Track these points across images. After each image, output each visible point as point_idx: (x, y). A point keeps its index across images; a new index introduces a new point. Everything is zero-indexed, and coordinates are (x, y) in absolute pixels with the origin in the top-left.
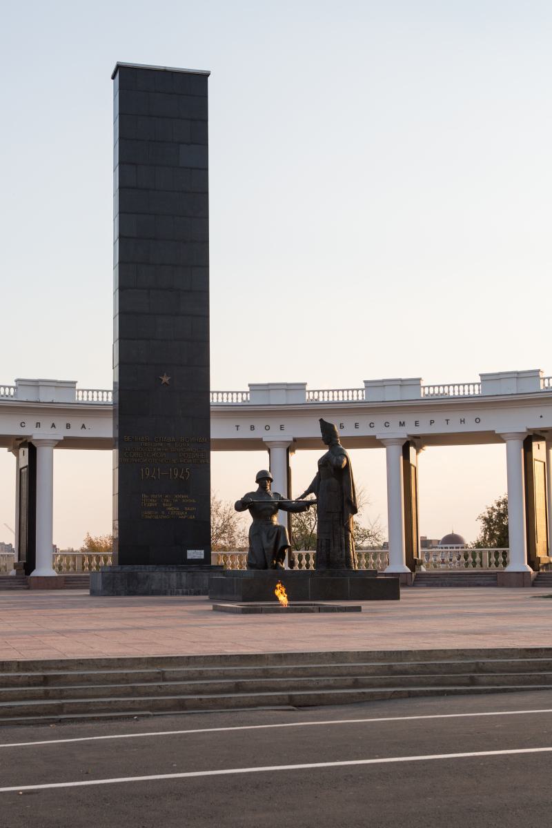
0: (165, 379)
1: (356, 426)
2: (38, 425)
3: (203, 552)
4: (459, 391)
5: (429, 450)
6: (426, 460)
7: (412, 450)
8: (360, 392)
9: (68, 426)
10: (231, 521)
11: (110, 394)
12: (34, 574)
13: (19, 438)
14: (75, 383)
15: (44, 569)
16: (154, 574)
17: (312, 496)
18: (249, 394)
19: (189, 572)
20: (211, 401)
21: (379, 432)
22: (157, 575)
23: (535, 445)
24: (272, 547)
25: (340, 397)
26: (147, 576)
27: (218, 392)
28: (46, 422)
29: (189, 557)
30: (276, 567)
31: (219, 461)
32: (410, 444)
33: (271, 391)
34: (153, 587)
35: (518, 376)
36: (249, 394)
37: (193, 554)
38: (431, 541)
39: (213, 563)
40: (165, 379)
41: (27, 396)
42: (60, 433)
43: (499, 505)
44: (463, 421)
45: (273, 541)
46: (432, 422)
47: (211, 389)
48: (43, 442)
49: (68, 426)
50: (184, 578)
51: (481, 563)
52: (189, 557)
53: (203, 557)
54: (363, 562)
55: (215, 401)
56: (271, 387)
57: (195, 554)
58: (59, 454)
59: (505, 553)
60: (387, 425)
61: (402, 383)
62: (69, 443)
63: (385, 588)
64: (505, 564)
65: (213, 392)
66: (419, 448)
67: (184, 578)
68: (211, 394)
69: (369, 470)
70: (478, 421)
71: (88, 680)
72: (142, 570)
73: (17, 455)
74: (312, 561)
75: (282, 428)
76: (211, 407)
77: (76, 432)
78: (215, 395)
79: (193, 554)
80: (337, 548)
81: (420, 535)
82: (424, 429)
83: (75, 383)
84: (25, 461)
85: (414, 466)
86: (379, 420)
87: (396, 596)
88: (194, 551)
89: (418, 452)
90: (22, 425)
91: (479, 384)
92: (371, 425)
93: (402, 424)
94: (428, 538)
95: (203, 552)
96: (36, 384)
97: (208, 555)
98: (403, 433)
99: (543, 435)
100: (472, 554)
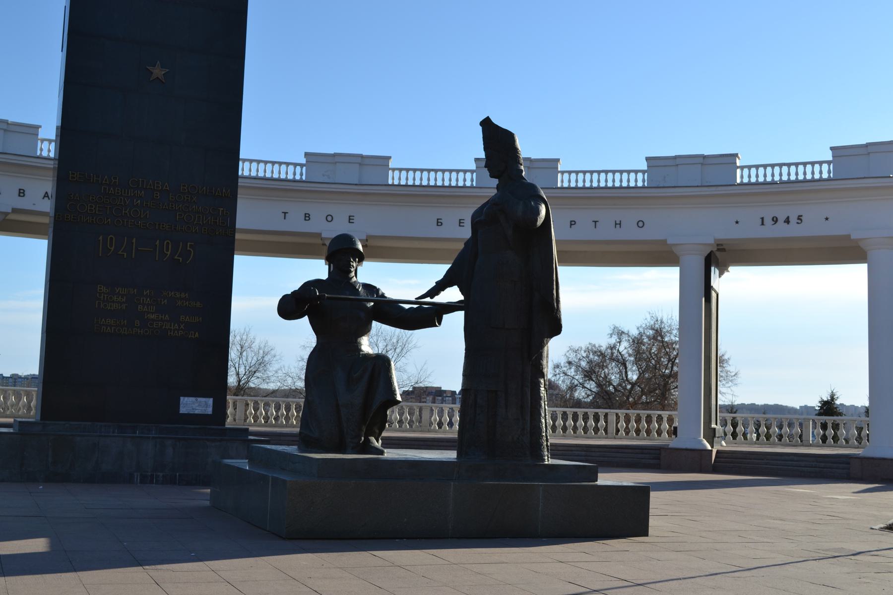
0: (158, 72)
3: (210, 401)
4: (457, 180)
5: (735, 272)
6: (735, 285)
7: (714, 272)
8: (468, 175)
10: (266, 359)
14: (38, 127)
17: (453, 294)
18: (304, 168)
20: (240, 173)
25: (610, 181)
27: (251, 161)
29: (183, 410)
30: (367, 448)
31: (244, 267)
32: (718, 257)
36: (304, 168)
37: (191, 405)
38: (445, 391)
39: (229, 423)
40: (158, 72)
46: (572, 223)
47: (242, 156)
51: (606, 430)
52: (183, 410)
53: (209, 411)
54: (435, 420)
55: (246, 173)
56: (678, 161)
57: (194, 405)
65: (244, 160)
68: (241, 163)
76: (240, 180)
78: (247, 164)
79: (191, 405)
81: (719, 403)
83: (38, 127)
85: (715, 291)
88: (193, 399)
89: (721, 274)
91: (643, 172)
94: (443, 389)
95: (210, 401)
100: (647, 417)
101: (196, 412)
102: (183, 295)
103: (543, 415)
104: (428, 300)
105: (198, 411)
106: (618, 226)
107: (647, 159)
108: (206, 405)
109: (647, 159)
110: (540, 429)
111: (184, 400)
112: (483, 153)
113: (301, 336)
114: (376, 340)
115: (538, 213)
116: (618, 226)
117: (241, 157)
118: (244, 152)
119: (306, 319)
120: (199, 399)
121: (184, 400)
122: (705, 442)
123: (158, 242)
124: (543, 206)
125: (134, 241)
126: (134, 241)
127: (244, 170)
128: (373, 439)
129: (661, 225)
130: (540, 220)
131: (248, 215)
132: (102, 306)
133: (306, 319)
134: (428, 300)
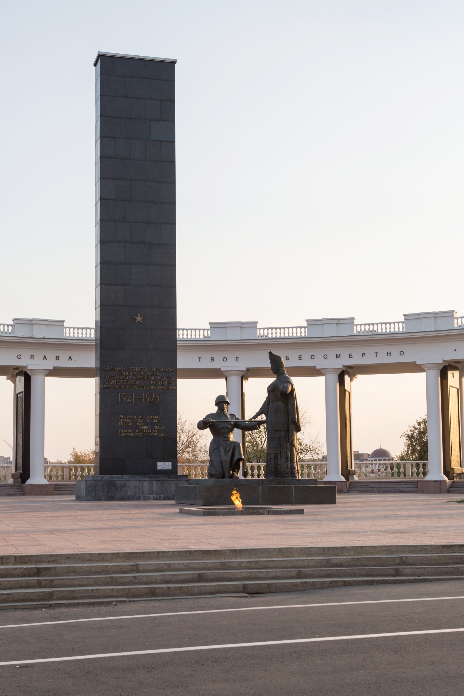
0: (139, 318)
1: (300, 358)
2: (32, 357)
3: (170, 464)
7: (347, 378)
9: (57, 358)
11: (93, 331)
12: (29, 482)
13: (16, 368)
15: (37, 478)
16: (129, 482)
17: (263, 417)
19: (159, 481)
20: (177, 337)
21: (319, 363)
22: (132, 483)
23: (450, 373)
24: (229, 459)
26: (124, 484)
28: (39, 355)
29: (159, 468)
32: (343, 374)
33: (228, 328)
34: (129, 493)
35: (436, 315)
40: (139, 318)
41: (23, 332)
42: (51, 364)
43: (419, 424)
44: (389, 354)
45: (230, 454)
46: (363, 355)
48: (36, 371)
49: (57, 358)
50: (155, 486)
52: (159, 468)
53: (170, 468)
58: (49, 381)
59: (424, 465)
60: (325, 357)
61: (338, 322)
62: (58, 372)
63: (324, 494)
64: (425, 474)
65: (179, 330)
66: (352, 377)
67: (155, 486)
68: (177, 331)
69: (310, 394)
70: (402, 353)
71: (74, 571)
72: (120, 479)
73: (14, 382)
74: (262, 472)
75: (237, 359)
76: (178, 342)
77: (64, 363)
80: (284, 460)
82: (357, 361)
84: (21, 388)
86: (319, 353)
87: (333, 501)
90: (19, 357)
92: (312, 357)
93: (338, 356)
95: (170, 464)
96: (31, 323)
97: (175, 466)
98: (339, 364)
99: (457, 365)
101: (165, 469)
102: (156, 417)
103: (295, 461)
104: (253, 420)
105: (165, 468)
106: (389, 355)
107: (405, 315)
108: (169, 466)
109: (405, 315)
110: (294, 468)
111: (159, 464)
112: (270, 364)
113: (206, 437)
114: (235, 436)
115: (288, 388)
116: (389, 355)
117: (177, 328)
118: (180, 324)
119: (208, 428)
120: (166, 463)
121: (159, 464)
122: (444, 476)
123: (144, 395)
124: (290, 386)
125: (134, 395)
126: (134, 395)
127: (180, 335)
128: (235, 473)
129: (412, 354)
130: (289, 391)
131: (183, 361)
132: (122, 424)
133: (208, 428)
134: (253, 420)
